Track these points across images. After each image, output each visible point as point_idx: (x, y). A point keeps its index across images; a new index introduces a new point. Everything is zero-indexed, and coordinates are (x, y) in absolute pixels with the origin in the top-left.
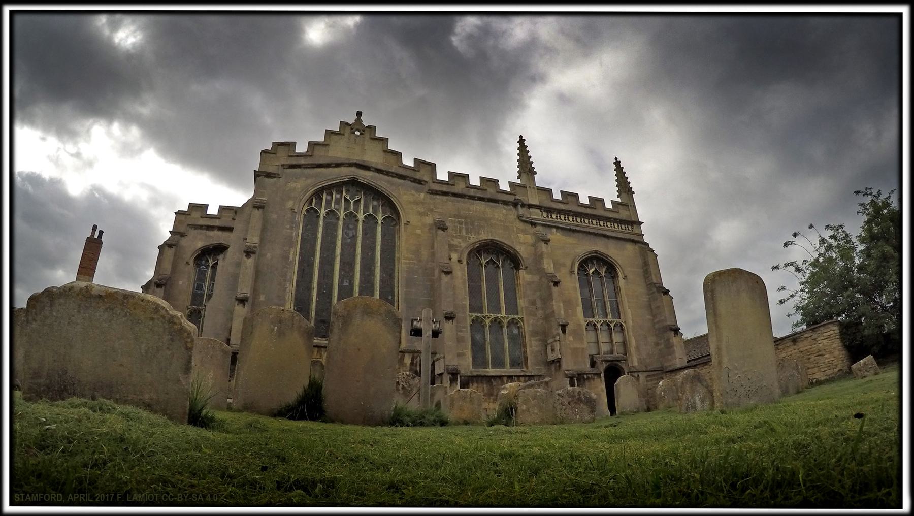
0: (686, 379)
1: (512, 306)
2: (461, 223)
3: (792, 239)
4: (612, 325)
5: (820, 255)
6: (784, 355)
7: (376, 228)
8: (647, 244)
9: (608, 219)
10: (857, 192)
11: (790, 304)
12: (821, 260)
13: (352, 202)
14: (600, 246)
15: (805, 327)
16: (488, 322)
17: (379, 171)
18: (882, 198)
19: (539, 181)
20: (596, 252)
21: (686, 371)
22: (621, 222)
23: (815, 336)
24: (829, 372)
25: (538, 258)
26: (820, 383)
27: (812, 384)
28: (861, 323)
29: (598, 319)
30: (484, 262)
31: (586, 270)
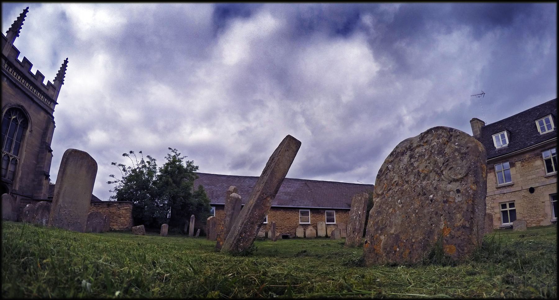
0: (41, 206)
3: (128, 153)
4: (11, 159)
5: (138, 168)
6: (101, 211)
8: (53, 118)
9: (39, 90)
10: (170, 149)
11: (113, 186)
12: (137, 170)
14: (25, 104)
15: (116, 200)
18: (180, 157)
19: (17, 43)
20: (22, 107)
21: (42, 202)
22: (46, 96)
23: (119, 206)
24: (121, 227)
26: (115, 231)
27: (111, 231)
28: (144, 208)
31: (10, 115)
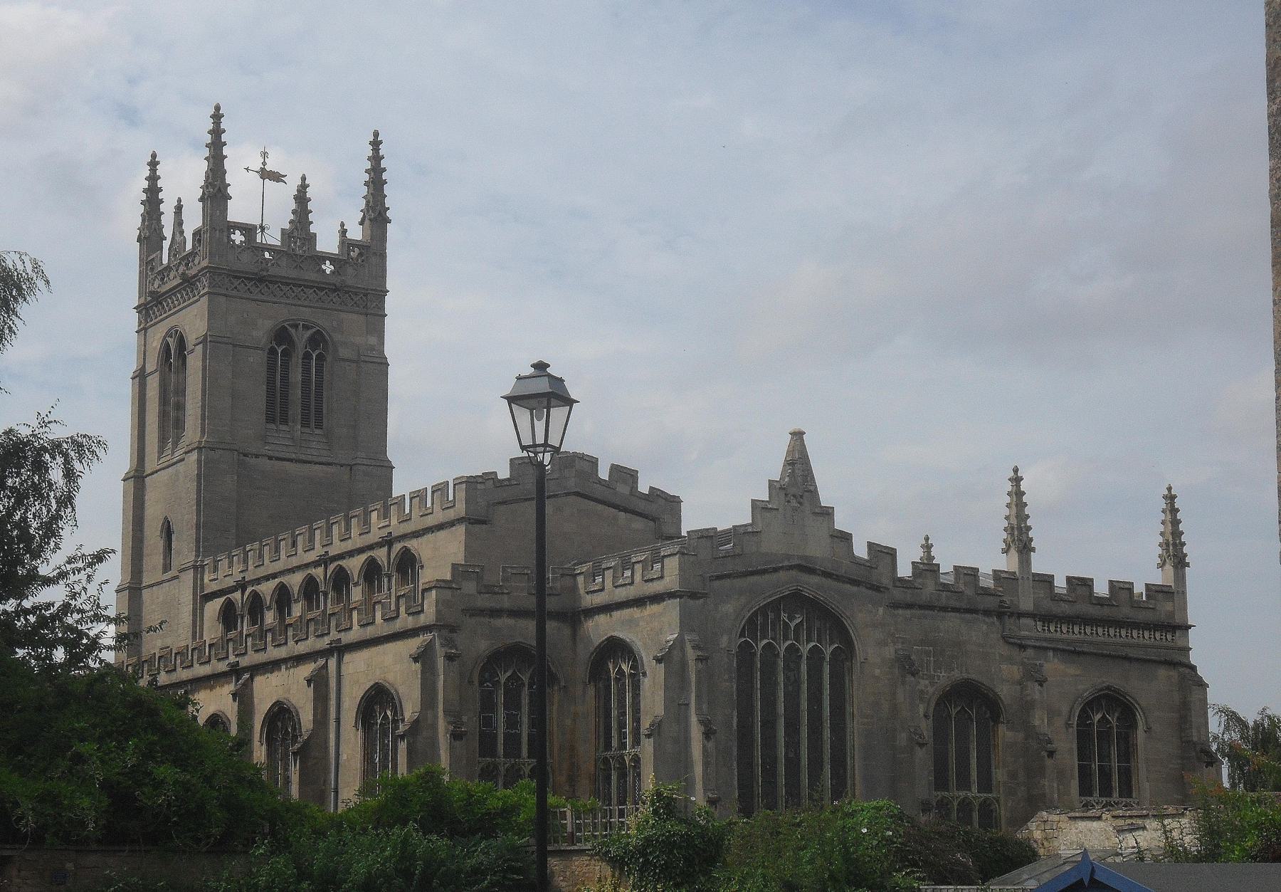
1: (986, 784)
2: (928, 654)
7: (822, 665)
8: (1193, 668)
13: (792, 625)
14: (1112, 677)
17: (827, 574)
20: (1108, 688)
25: (1027, 706)
30: (954, 713)
31: (1089, 717)
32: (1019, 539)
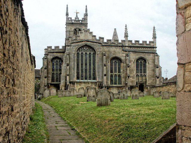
1: (119, 72)
14: (142, 55)
16: (114, 75)
20: (141, 57)
29: (139, 74)
31: (138, 62)
32: (126, 36)
